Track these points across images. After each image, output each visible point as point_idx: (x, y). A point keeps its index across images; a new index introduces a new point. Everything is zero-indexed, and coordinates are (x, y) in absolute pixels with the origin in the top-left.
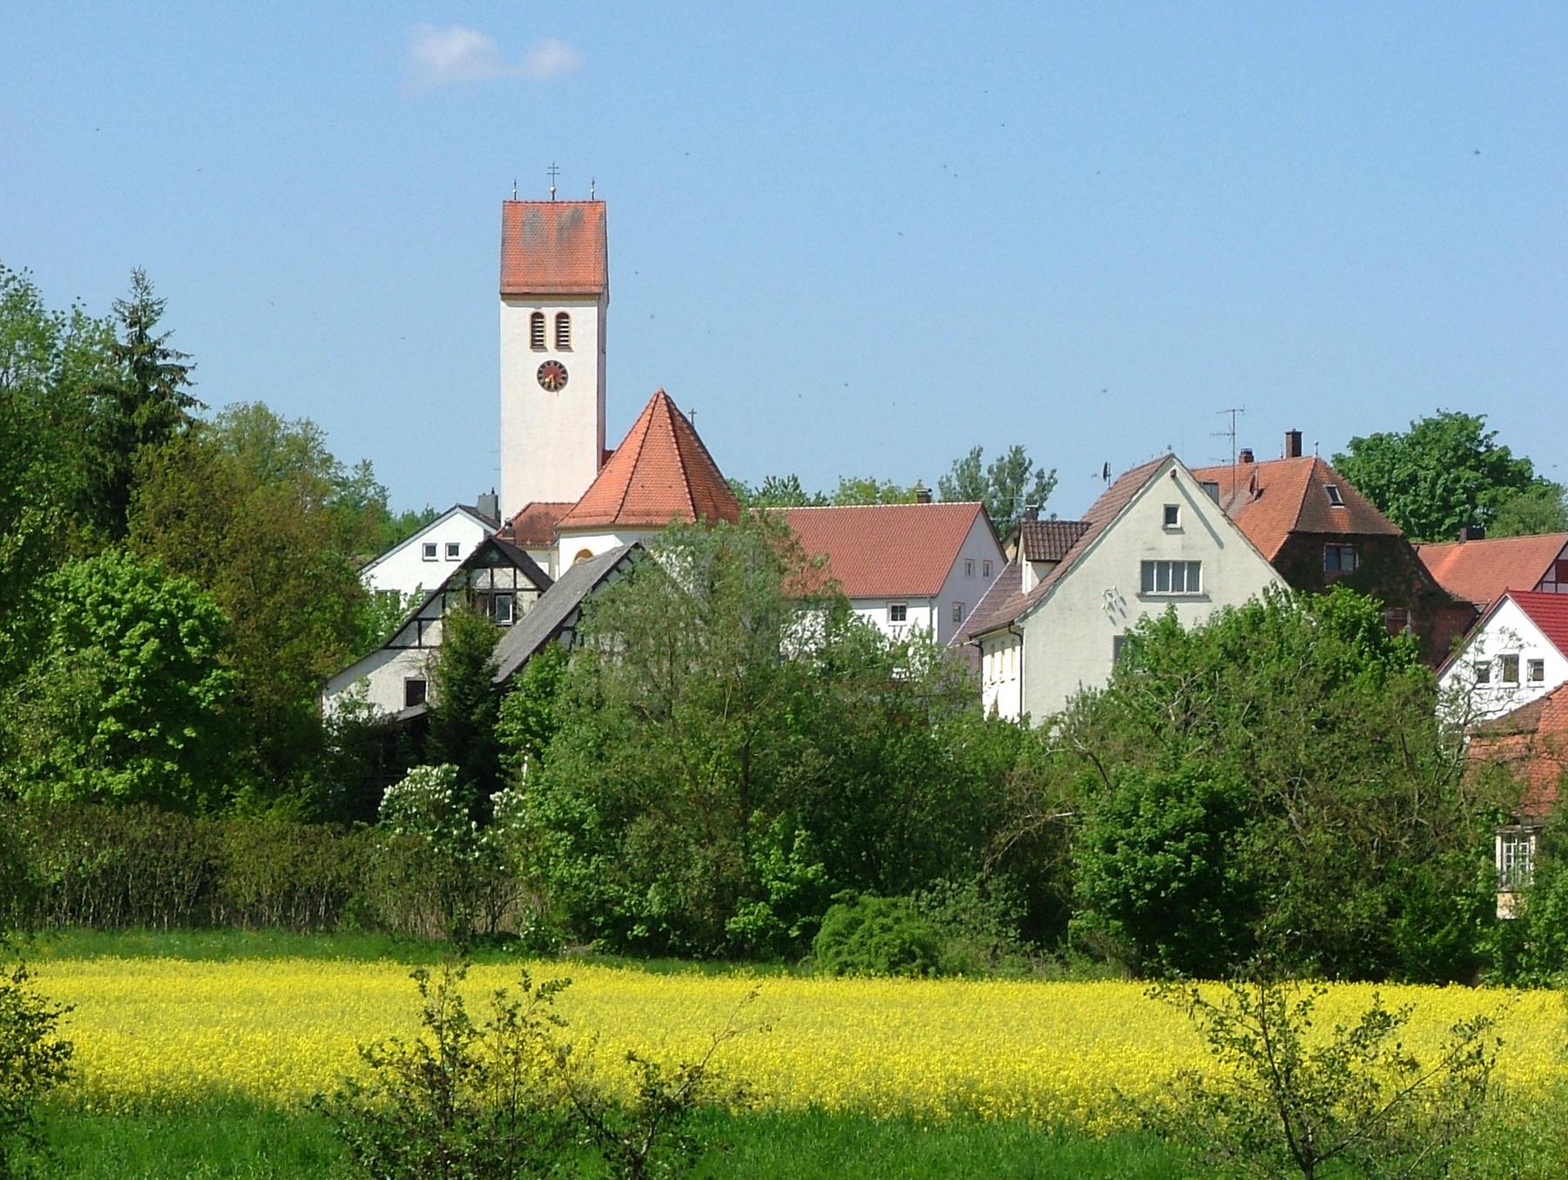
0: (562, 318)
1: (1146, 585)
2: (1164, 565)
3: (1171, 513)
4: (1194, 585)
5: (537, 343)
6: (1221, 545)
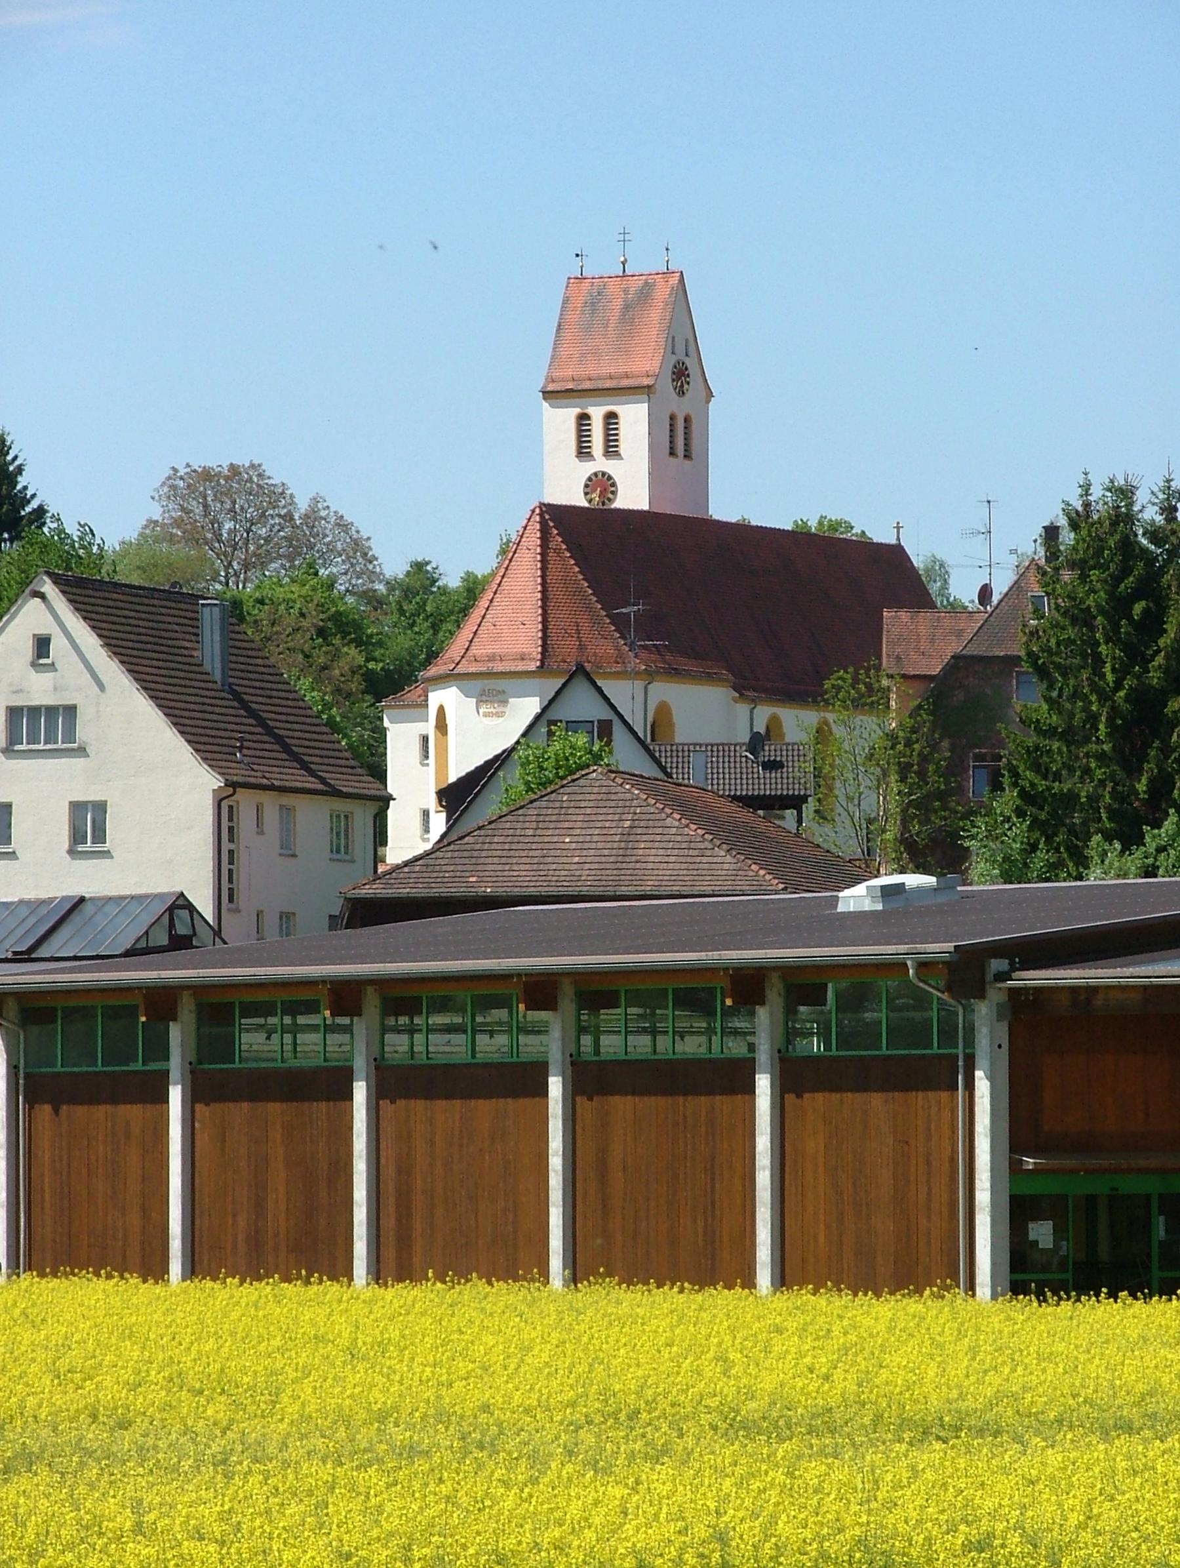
0: (611, 417)
1: (13, 737)
2: (34, 711)
3: (42, 645)
4: (70, 735)
5: (583, 451)
6: (101, 687)
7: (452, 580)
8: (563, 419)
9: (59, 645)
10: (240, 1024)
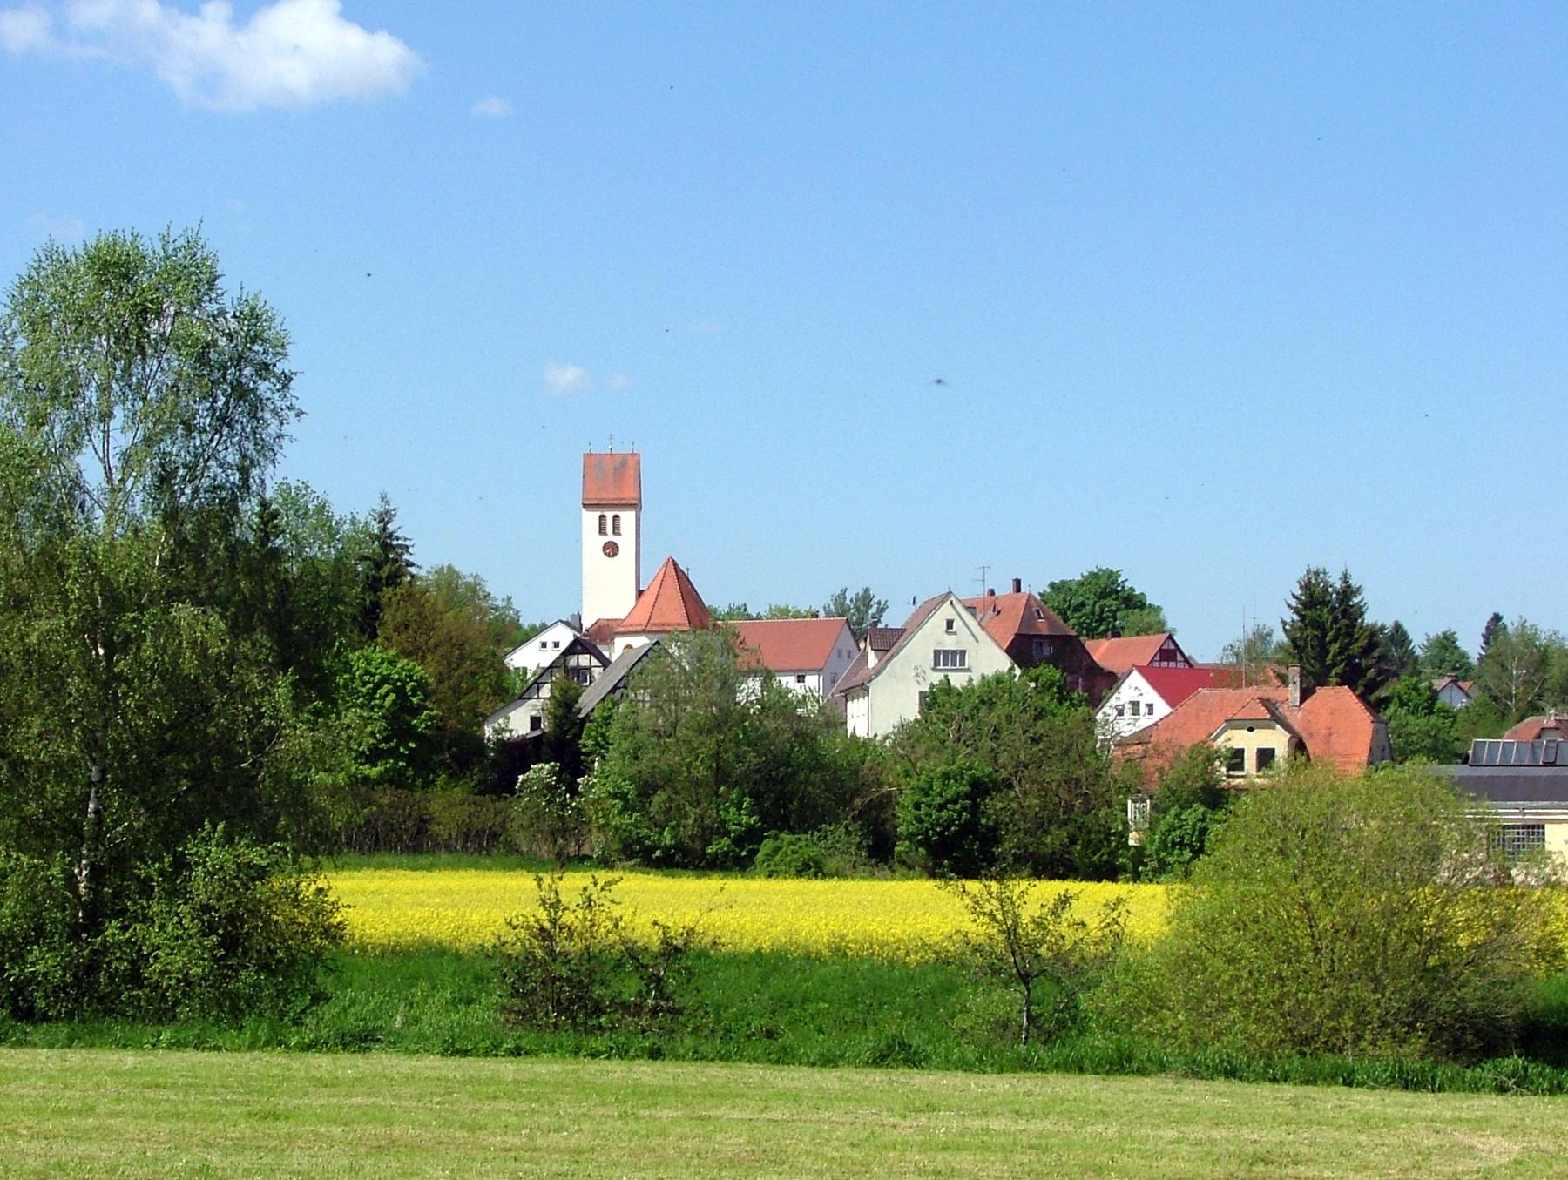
2: (946, 652)
3: (950, 624)
5: (602, 531)
7: (525, 622)
8: (591, 518)
9: (957, 624)
10: (1546, 765)
